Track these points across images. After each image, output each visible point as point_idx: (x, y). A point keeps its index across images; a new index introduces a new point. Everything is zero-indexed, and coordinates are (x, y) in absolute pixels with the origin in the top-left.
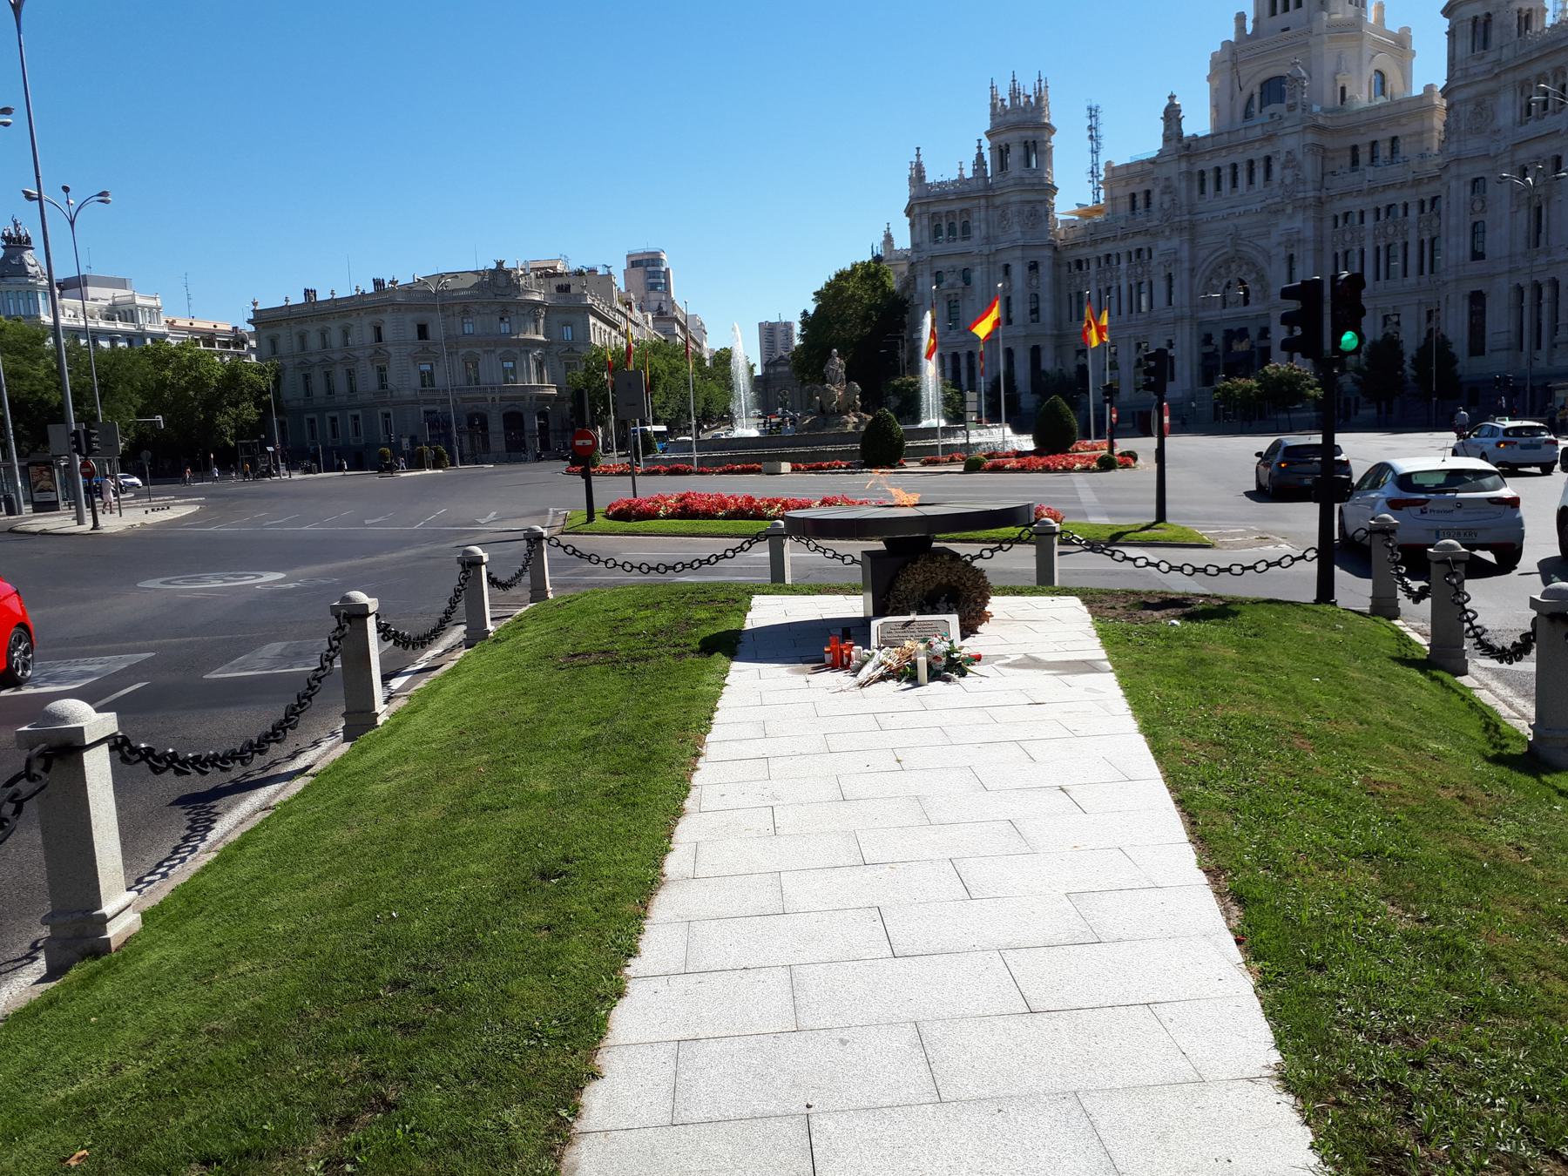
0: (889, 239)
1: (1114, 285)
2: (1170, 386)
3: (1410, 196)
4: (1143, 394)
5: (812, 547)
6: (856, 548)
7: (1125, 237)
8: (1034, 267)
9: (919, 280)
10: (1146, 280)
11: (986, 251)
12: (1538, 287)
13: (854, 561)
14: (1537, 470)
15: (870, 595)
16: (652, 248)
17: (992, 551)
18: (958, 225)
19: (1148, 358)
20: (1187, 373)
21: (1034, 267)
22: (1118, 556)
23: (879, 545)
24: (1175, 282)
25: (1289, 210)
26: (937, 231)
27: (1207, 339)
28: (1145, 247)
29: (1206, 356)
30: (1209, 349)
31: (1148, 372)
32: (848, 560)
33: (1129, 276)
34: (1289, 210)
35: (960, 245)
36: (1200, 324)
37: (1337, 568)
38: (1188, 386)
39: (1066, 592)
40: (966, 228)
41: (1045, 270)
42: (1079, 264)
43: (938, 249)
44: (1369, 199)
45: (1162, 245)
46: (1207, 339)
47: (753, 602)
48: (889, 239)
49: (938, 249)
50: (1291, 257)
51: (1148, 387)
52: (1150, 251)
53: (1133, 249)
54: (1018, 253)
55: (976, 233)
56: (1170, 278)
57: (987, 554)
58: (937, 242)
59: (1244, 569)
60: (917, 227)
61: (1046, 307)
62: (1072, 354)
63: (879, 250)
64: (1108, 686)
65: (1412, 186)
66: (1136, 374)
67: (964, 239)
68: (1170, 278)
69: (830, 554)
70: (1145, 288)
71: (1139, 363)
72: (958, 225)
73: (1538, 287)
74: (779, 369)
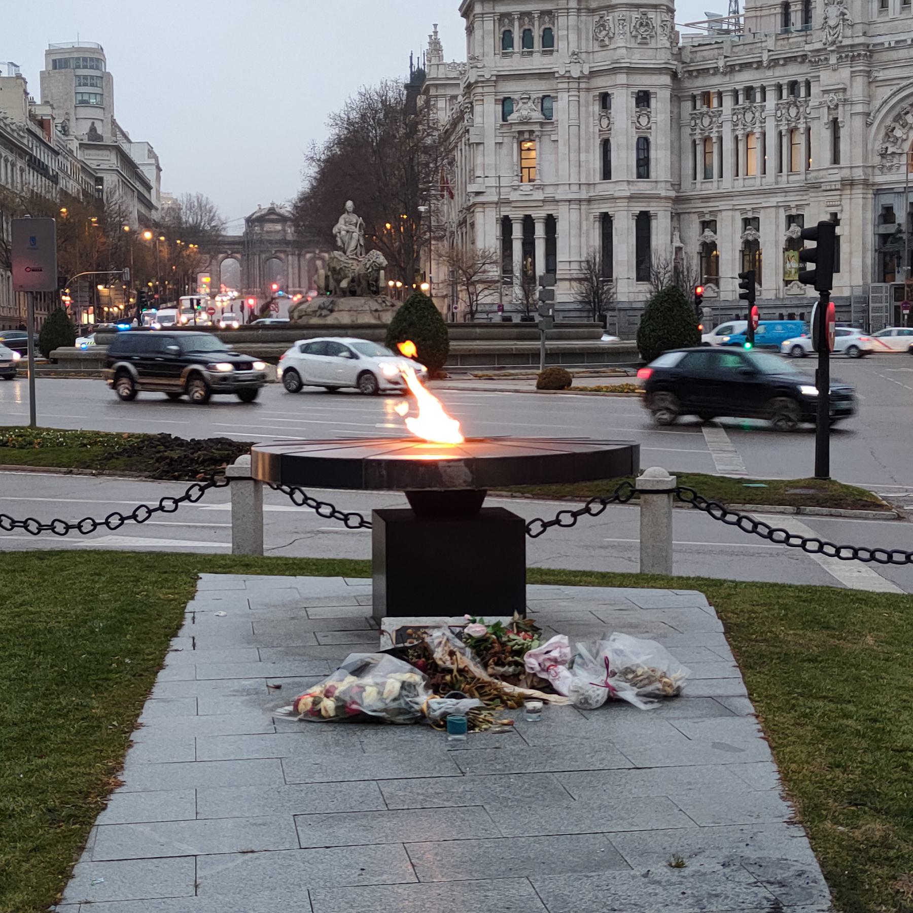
0: (435, 47)
1: (714, 135)
2: (836, 279)
3: (770, 77)
4: (796, 288)
5: (298, 497)
6: (365, 502)
7: (774, 63)
8: (643, 99)
9: (478, 109)
10: (802, 127)
11: (575, 73)
12: (528, 223)
13: (362, 524)
14: (233, 398)
15: (382, 580)
16: (87, 39)
17: (575, 515)
18: (537, 33)
19: (808, 234)
20: (857, 262)
21: (643, 99)
22: (298, 497)
23: (397, 500)
24: (843, 133)
25: (833, 60)
26: (507, 41)
27: (887, 215)
28: (801, 79)
29: (884, 238)
30: (891, 229)
31: (805, 257)
32: (354, 521)
33: (778, 120)
34: (833, 60)
35: (538, 62)
36: (878, 193)
37: (409, 506)
38: (858, 280)
39: (686, 583)
40: (548, 40)
41: (661, 106)
42: (706, 97)
43: (516, 63)
44: (769, 73)
45: (827, 78)
46: (887, 215)
47: (200, 584)
48: (435, 47)
49: (516, 63)
50: (835, 122)
51: (805, 278)
52: (808, 84)
53: (784, 81)
54: (622, 79)
55: (561, 45)
56: (835, 125)
57: (566, 519)
58: (505, 55)
59: (557, 522)
60: (478, 33)
61: (660, 157)
62: (696, 226)
63: (420, 63)
64: (745, 731)
65: (724, 74)
66: (786, 260)
67: (544, 53)
68: (835, 125)
69: (325, 510)
70: (800, 139)
71: (792, 244)
72: (537, 33)
73: (528, 223)
74: (268, 227)
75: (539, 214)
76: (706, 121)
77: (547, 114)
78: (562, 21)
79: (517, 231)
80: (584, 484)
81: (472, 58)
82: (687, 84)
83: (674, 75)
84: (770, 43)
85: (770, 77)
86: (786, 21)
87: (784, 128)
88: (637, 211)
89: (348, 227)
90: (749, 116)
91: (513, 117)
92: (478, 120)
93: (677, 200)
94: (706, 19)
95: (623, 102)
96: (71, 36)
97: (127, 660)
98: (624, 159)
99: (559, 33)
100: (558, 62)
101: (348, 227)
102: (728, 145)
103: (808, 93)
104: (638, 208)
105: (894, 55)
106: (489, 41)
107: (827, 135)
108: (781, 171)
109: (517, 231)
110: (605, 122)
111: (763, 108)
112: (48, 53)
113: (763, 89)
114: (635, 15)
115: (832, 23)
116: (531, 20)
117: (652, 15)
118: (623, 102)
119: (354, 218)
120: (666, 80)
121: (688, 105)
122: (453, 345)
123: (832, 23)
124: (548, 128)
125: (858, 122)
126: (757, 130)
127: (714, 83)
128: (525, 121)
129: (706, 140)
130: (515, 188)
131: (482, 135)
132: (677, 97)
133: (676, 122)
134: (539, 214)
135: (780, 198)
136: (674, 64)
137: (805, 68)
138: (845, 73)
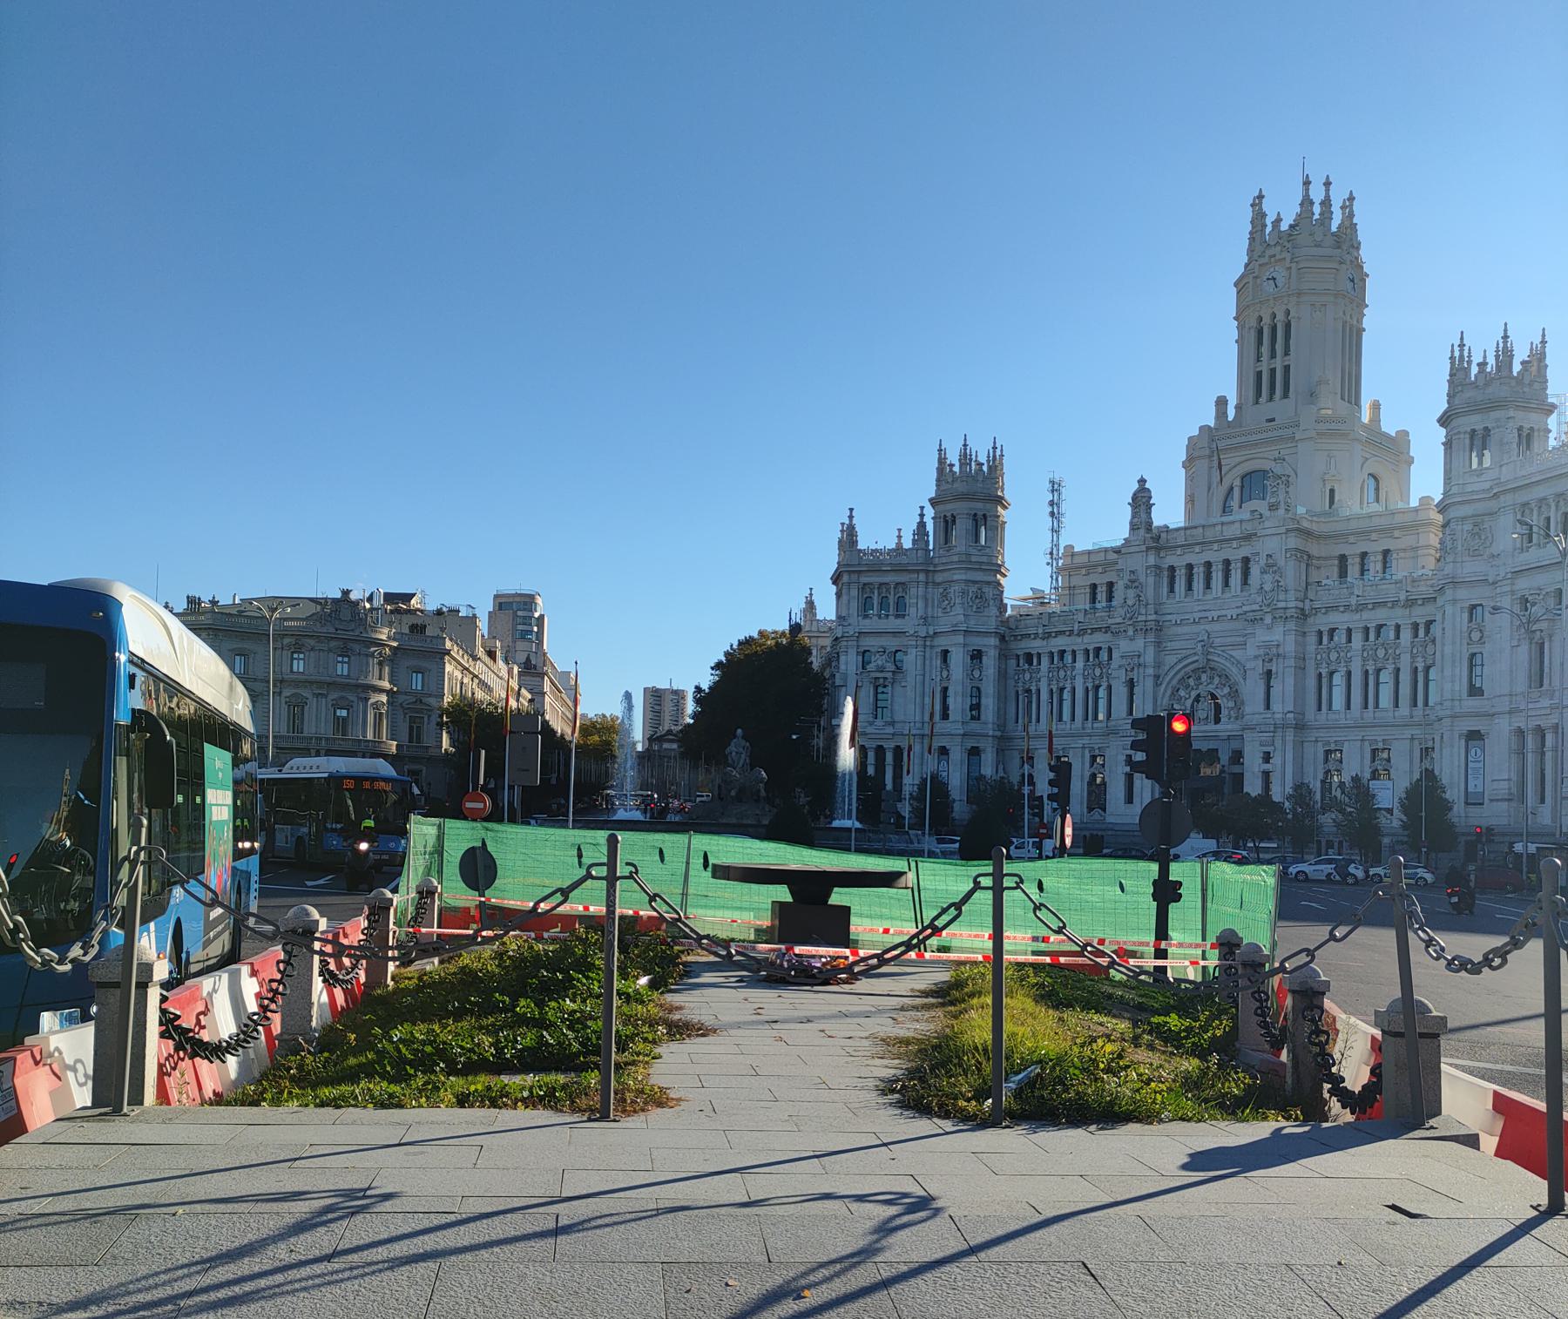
0: (810, 605)
1: (1033, 689)
3: (1079, 643)
8: (977, 656)
9: (842, 658)
21: (977, 656)
35: (893, 624)
41: (990, 661)
42: (1029, 658)
45: (1124, 646)
48: (810, 605)
50: (1269, 673)
54: (960, 639)
56: (1131, 684)
58: (866, 617)
60: (845, 598)
61: (989, 703)
67: (897, 616)
68: (1131, 684)
73: (880, 751)
75: (889, 745)
76: (1027, 676)
77: (899, 668)
78: (913, 591)
79: (871, 756)
80: (1095, 1017)
81: (839, 617)
82: (1013, 645)
83: (1002, 638)
84: (1080, 617)
85: (1079, 643)
86: (1093, 600)
87: (1090, 686)
88: (969, 746)
89: (738, 748)
90: (1062, 673)
91: (871, 667)
92: (842, 667)
93: (1001, 738)
94: (1030, 594)
95: (958, 659)
96: (512, 586)
97: (416, 791)
98: (957, 703)
99: (910, 600)
100: (909, 624)
101: (738, 748)
102: (1044, 696)
103: (1110, 658)
104: (970, 744)
105: (1179, 630)
106: (854, 604)
107: (1124, 691)
108: (1415, 705)
109: (871, 756)
110: (945, 674)
111: (1073, 668)
112: (496, 597)
113: (1039, 655)
114: (973, 589)
115: (1130, 602)
116: (888, 591)
117: (985, 589)
118: (958, 659)
119: (743, 742)
120: (993, 641)
121: (1013, 662)
122: (370, 736)
123: (1130, 602)
124: (899, 676)
125: (1150, 683)
126: (1068, 686)
127: (1035, 645)
128: (881, 669)
129: (1029, 691)
130: (871, 724)
131: (845, 680)
132: (1003, 656)
133: (1002, 675)
134: (889, 745)
135: (1086, 741)
136: (1002, 630)
137: (1108, 636)
138: (1139, 643)
